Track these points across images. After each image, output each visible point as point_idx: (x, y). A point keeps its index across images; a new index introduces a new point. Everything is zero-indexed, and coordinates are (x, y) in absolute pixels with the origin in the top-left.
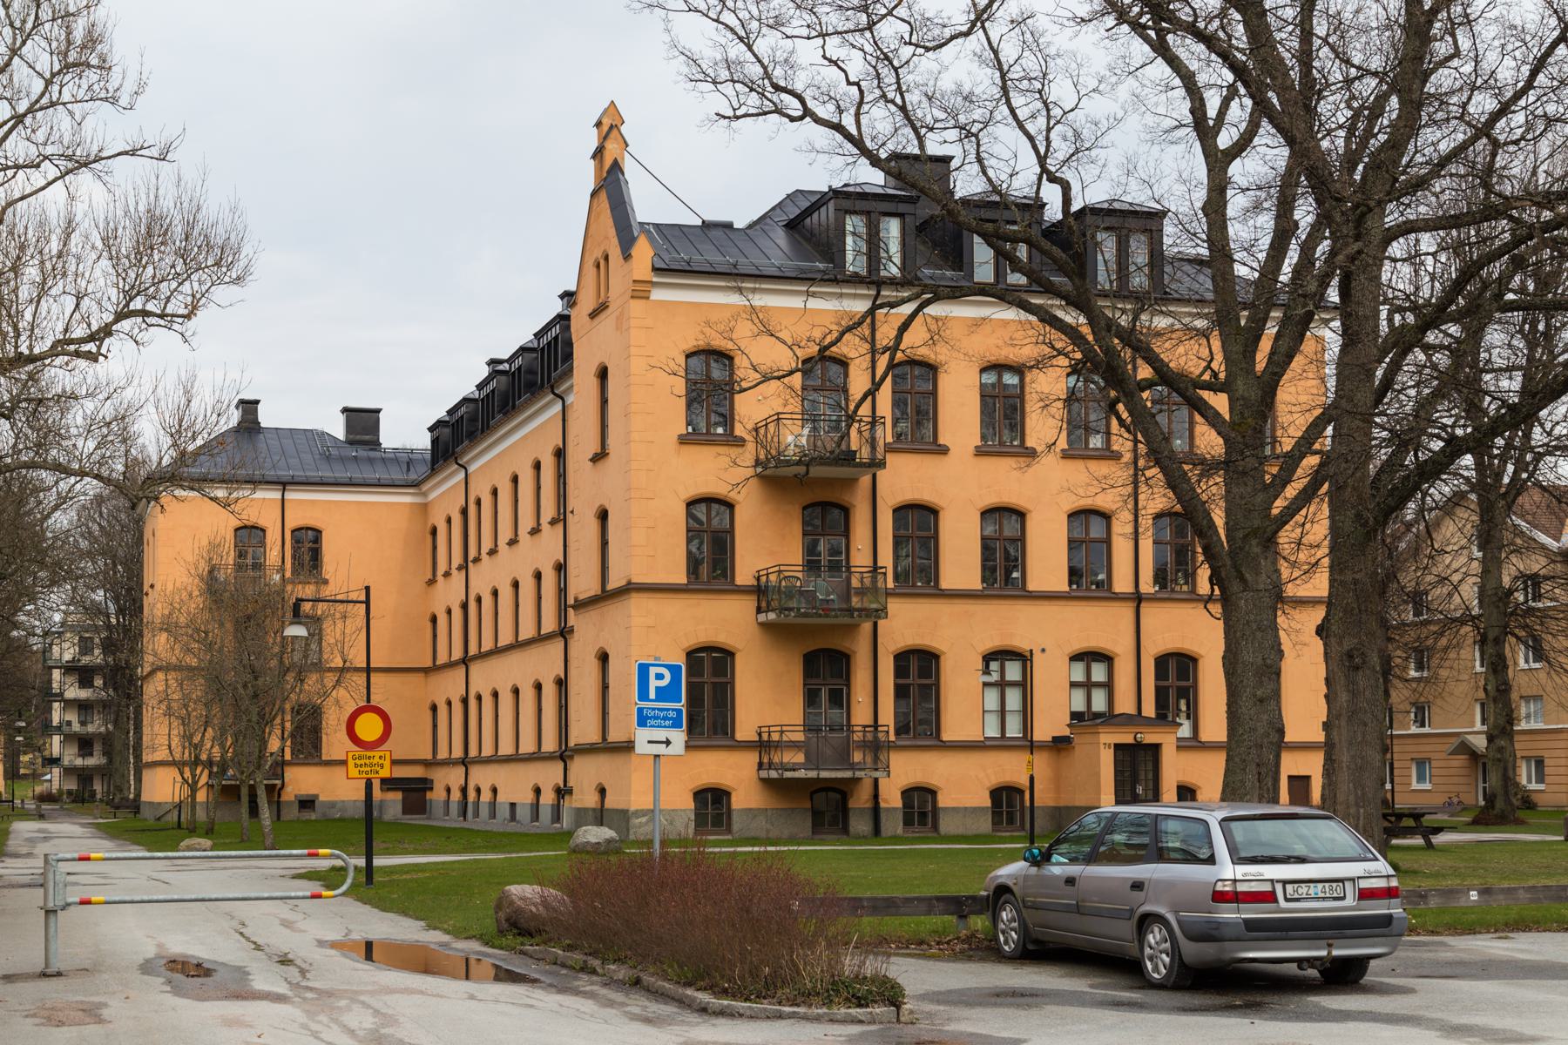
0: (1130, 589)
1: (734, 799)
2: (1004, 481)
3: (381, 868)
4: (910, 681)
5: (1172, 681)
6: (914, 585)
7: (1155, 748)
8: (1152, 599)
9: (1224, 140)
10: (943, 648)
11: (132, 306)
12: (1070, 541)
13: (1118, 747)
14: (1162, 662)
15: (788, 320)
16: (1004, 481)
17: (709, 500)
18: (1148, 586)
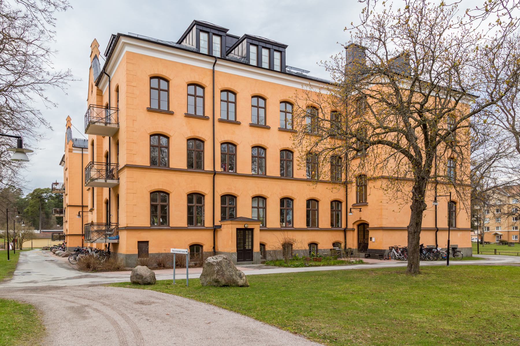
0: (211, 169)
1: (204, 248)
2: (259, 137)
3: (422, 267)
4: (157, 203)
5: (195, 203)
6: (228, 171)
7: (252, 230)
8: (220, 173)
9: (499, 72)
10: (296, 197)
11: (457, 121)
12: (151, 146)
13: (237, 229)
14: (224, 197)
15: (182, 70)
16: (259, 137)
17: (228, 143)
18: (218, 169)
